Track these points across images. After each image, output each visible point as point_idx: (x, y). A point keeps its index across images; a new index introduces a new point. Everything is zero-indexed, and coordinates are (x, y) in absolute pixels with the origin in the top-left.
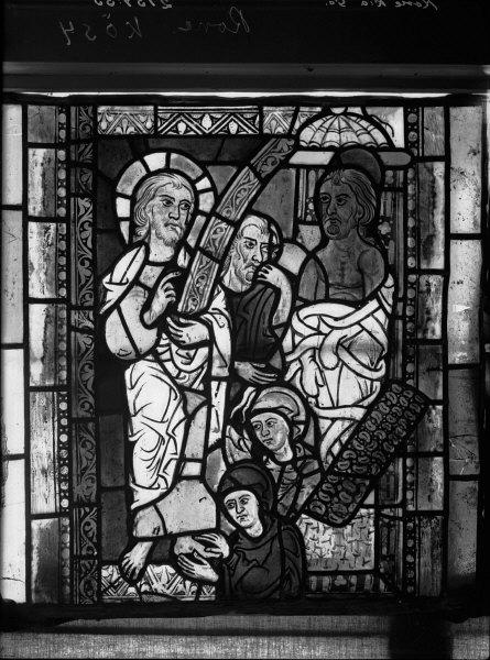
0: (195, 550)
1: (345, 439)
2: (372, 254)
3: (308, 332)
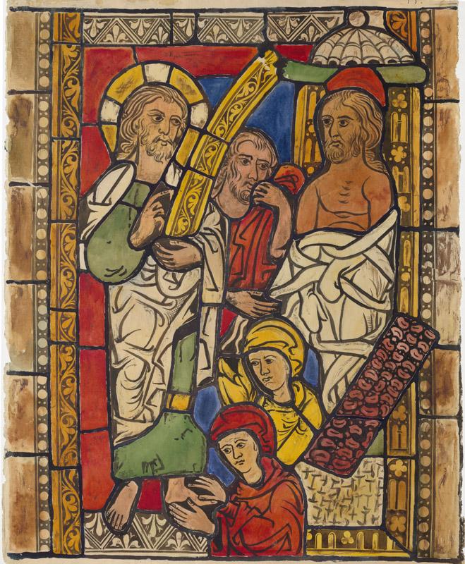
0: (189, 498)
1: (351, 377)
2: (379, 182)
3: (308, 263)
